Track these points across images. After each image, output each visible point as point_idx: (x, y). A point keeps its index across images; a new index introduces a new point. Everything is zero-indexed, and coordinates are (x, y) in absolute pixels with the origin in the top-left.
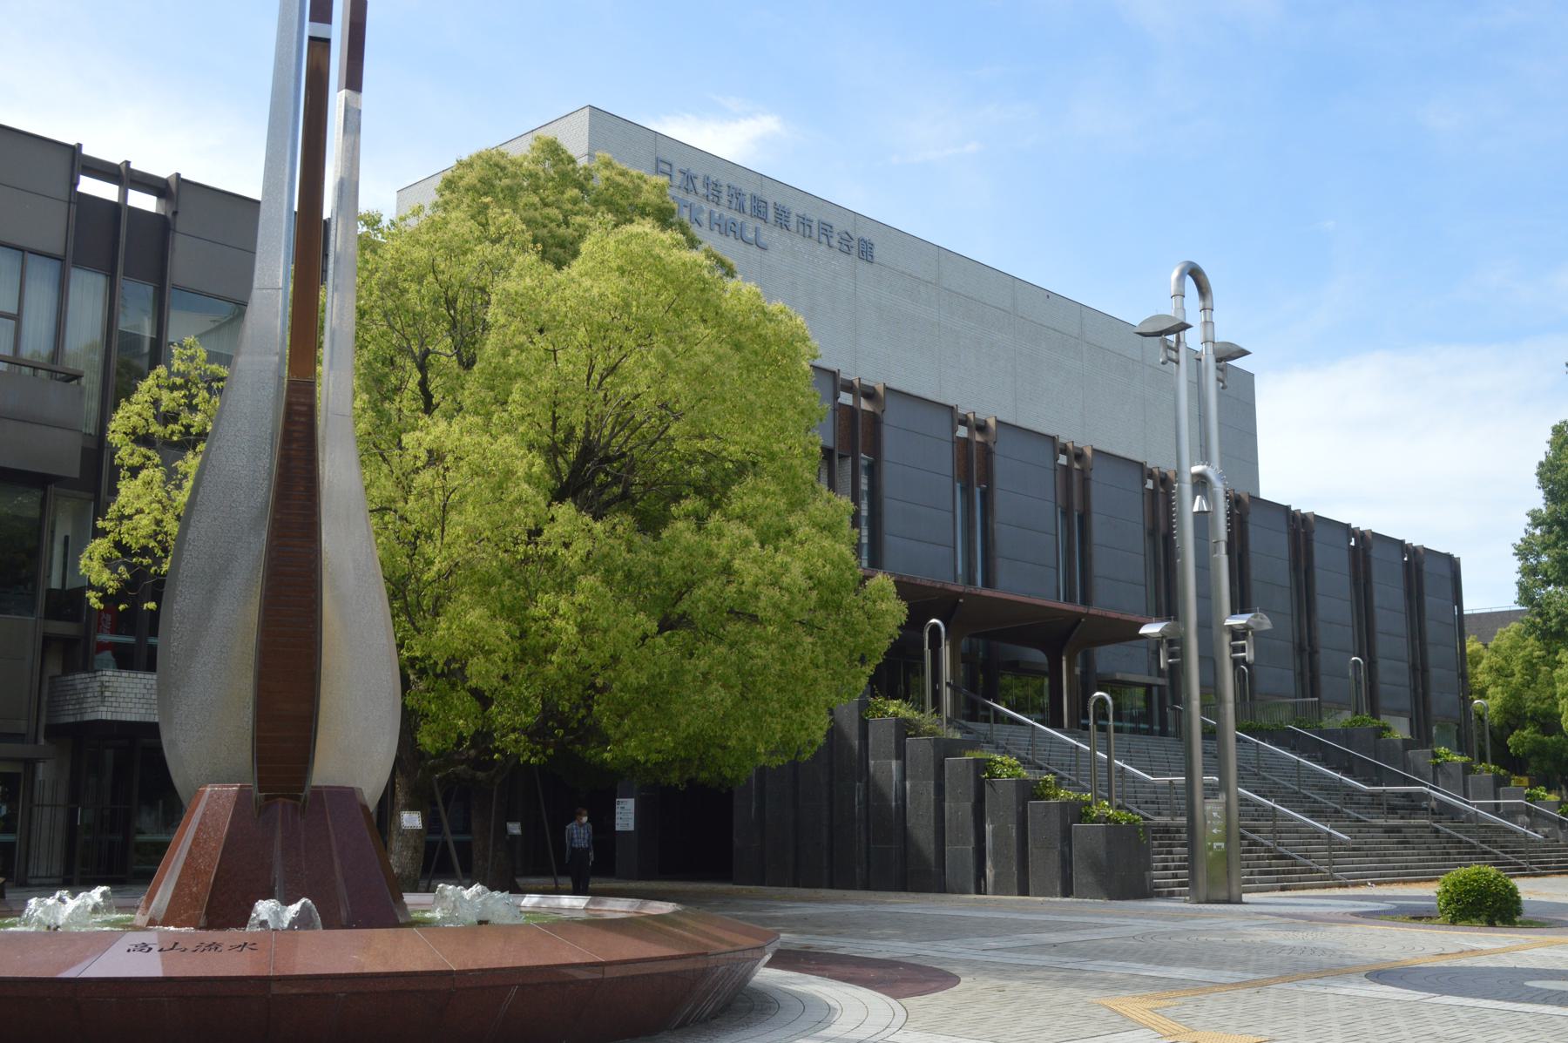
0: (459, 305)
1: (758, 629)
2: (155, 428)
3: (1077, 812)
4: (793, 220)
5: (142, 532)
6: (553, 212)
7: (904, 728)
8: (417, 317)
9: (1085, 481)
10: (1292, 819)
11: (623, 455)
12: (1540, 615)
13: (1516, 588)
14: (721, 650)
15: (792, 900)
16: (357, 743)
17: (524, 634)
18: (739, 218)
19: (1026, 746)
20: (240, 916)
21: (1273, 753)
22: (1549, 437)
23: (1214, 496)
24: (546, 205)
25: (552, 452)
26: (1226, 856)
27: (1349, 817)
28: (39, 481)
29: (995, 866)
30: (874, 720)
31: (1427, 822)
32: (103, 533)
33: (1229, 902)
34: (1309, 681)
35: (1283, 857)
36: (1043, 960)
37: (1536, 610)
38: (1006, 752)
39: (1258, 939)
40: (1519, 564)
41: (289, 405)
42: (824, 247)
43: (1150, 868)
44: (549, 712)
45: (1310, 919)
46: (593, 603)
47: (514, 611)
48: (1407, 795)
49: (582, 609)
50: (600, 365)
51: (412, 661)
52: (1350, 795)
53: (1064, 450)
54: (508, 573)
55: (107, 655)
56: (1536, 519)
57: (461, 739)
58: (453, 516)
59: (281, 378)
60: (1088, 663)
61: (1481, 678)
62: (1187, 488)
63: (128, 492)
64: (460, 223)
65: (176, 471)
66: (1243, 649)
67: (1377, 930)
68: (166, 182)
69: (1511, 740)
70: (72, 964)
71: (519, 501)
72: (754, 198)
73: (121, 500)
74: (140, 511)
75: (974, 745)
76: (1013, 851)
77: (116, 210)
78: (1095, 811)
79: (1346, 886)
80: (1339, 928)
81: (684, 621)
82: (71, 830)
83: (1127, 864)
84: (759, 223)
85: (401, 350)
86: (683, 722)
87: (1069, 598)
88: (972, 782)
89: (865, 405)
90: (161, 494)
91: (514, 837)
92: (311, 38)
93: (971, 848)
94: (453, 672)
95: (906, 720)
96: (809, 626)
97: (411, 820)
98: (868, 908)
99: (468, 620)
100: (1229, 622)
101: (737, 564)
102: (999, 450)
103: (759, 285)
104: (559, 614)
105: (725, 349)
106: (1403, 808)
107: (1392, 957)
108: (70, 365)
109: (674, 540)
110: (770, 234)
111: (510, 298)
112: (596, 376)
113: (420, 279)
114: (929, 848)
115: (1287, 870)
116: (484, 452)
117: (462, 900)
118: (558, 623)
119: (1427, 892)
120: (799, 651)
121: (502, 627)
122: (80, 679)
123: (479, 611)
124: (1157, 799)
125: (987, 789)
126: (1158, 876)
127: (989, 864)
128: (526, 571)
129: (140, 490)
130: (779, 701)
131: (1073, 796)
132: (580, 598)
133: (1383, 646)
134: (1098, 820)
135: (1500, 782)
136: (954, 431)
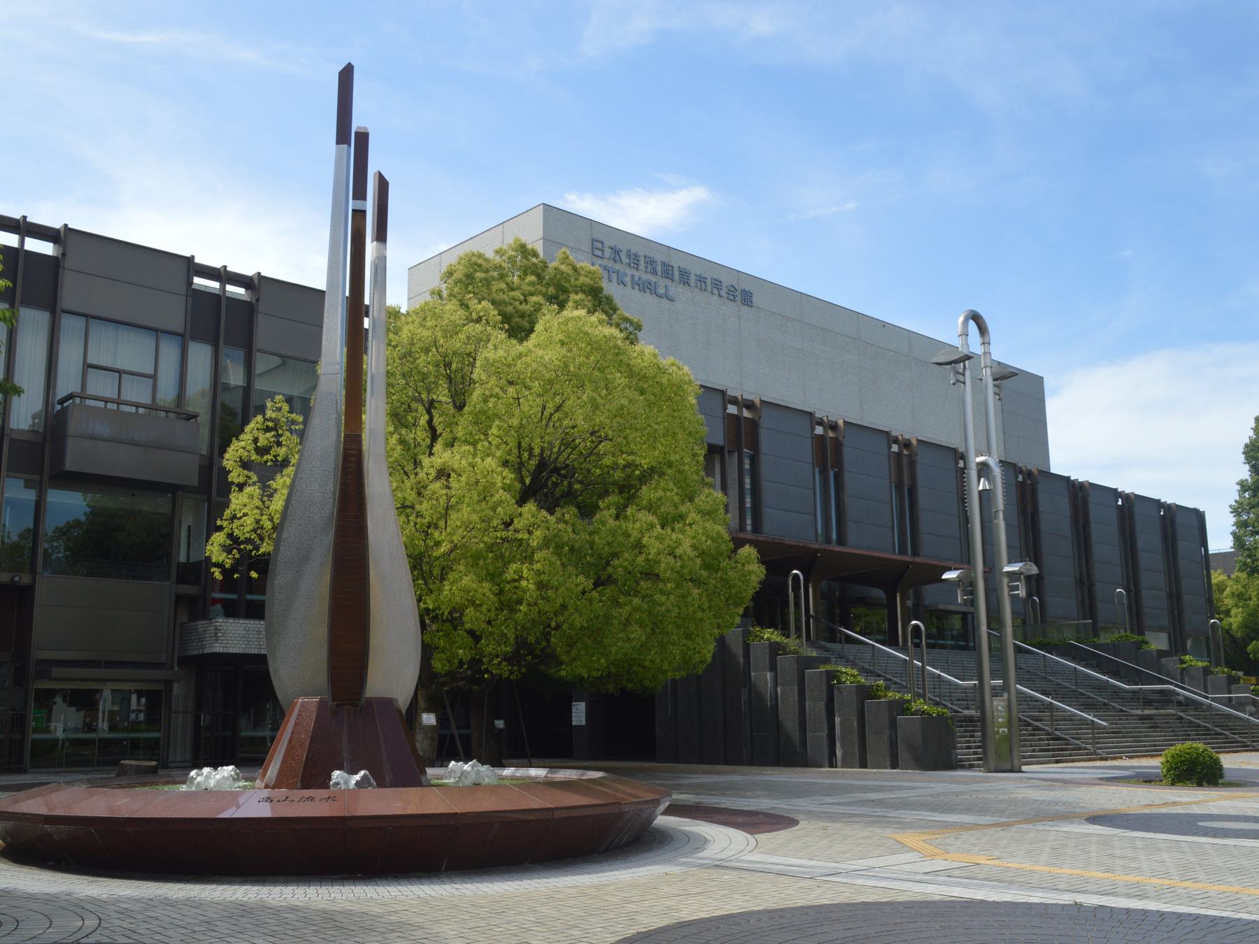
0: (454, 366)
1: (661, 585)
2: (254, 457)
3: (901, 708)
4: (693, 278)
5: (247, 529)
6: (517, 294)
7: (775, 649)
8: (424, 377)
9: (912, 464)
10: (1065, 711)
11: (567, 466)
12: (1249, 556)
13: (1231, 538)
14: (636, 601)
15: (696, 772)
16: (394, 670)
17: (501, 592)
18: (653, 279)
19: (876, 661)
20: (324, 783)
21: (1058, 662)
22: (1253, 425)
23: (994, 477)
24: (513, 289)
25: (519, 468)
26: (1008, 738)
27: (1114, 708)
28: (171, 489)
29: (843, 746)
30: (754, 643)
31: (1173, 712)
32: (220, 528)
33: (1012, 771)
34: (1088, 606)
35: (1058, 739)
36: (862, 810)
37: (1246, 553)
38: (853, 665)
39: (1020, 796)
40: (1234, 519)
41: (345, 450)
42: (715, 297)
43: (956, 748)
44: (521, 643)
45: (1065, 782)
46: (547, 568)
47: (494, 577)
48: (1161, 692)
49: (538, 573)
50: (551, 407)
51: (427, 610)
52: (1117, 691)
53: (896, 441)
54: (490, 548)
55: (218, 607)
56: (1243, 486)
57: (461, 663)
58: (453, 515)
59: (339, 432)
60: (918, 597)
61: (1226, 601)
62: (973, 473)
63: (237, 501)
64: (451, 310)
65: (269, 487)
66: (1017, 588)
67: (1111, 789)
68: (250, 278)
69: (1250, 648)
70: (223, 810)
71: (500, 502)
72: (664, 264)
73: (232, 506)
74: (245, 515)
75: (826, 661)
76: (855, 738)
77: (217, 299)
78: (914, 707)
79: (1106, 759)
80: (1084, 789)
81: (610, 580)
82: (197, 728)
83: (936, 747)
84: (668, 282)
85: (414, 399)
86: (613, 650)
87: (903, 551)
88: (824, 687)
89: (746, 413)
90: (259, 503)
91: (500, 730)
92: (354, 211)
93: (824, 734)
94: (454, 619)
95: (776, 643)
96: (695, 581)
97: (429, 719)
98: (748, 778)
99: (463, 583)
100: (1007, 569)
101: (645, 541)
102: (847, 443)
103: (657, 347)
104: (525, 576)
105: (636, 395)
106: (1158, 702)
107: (1113, 807)
108: (190, 409)
109: (603, 523)
110: (676, 290)
111: (488, 364)
112: (547, 413)
113: (427, 351)
114: (795, 735)
115: (1061, 746)
116: (474, 470)
117: (461, 770)
118: (524, 583)
119: (1154, 764)
120: (690, 599)
121: (486, 585)
122: (201, 625)
123: (471, 577)
124: (966, 697)
125: (836, 692)
126: (961, 753)
127: (838, 745)
128: (496, 556)
129: (246, 500)
130: (677, 635)
131: (898, 696)
132: (537, 566)
133: (1146, 579)
134: (916, 713)
135: (1232, 681)
136: (813, 430)
